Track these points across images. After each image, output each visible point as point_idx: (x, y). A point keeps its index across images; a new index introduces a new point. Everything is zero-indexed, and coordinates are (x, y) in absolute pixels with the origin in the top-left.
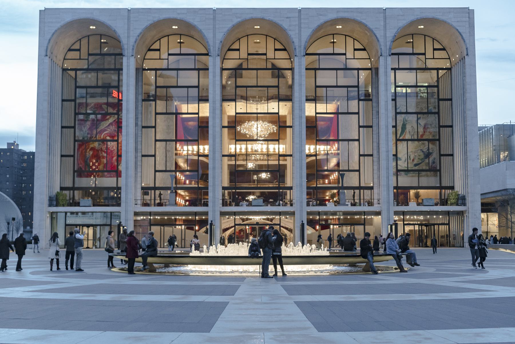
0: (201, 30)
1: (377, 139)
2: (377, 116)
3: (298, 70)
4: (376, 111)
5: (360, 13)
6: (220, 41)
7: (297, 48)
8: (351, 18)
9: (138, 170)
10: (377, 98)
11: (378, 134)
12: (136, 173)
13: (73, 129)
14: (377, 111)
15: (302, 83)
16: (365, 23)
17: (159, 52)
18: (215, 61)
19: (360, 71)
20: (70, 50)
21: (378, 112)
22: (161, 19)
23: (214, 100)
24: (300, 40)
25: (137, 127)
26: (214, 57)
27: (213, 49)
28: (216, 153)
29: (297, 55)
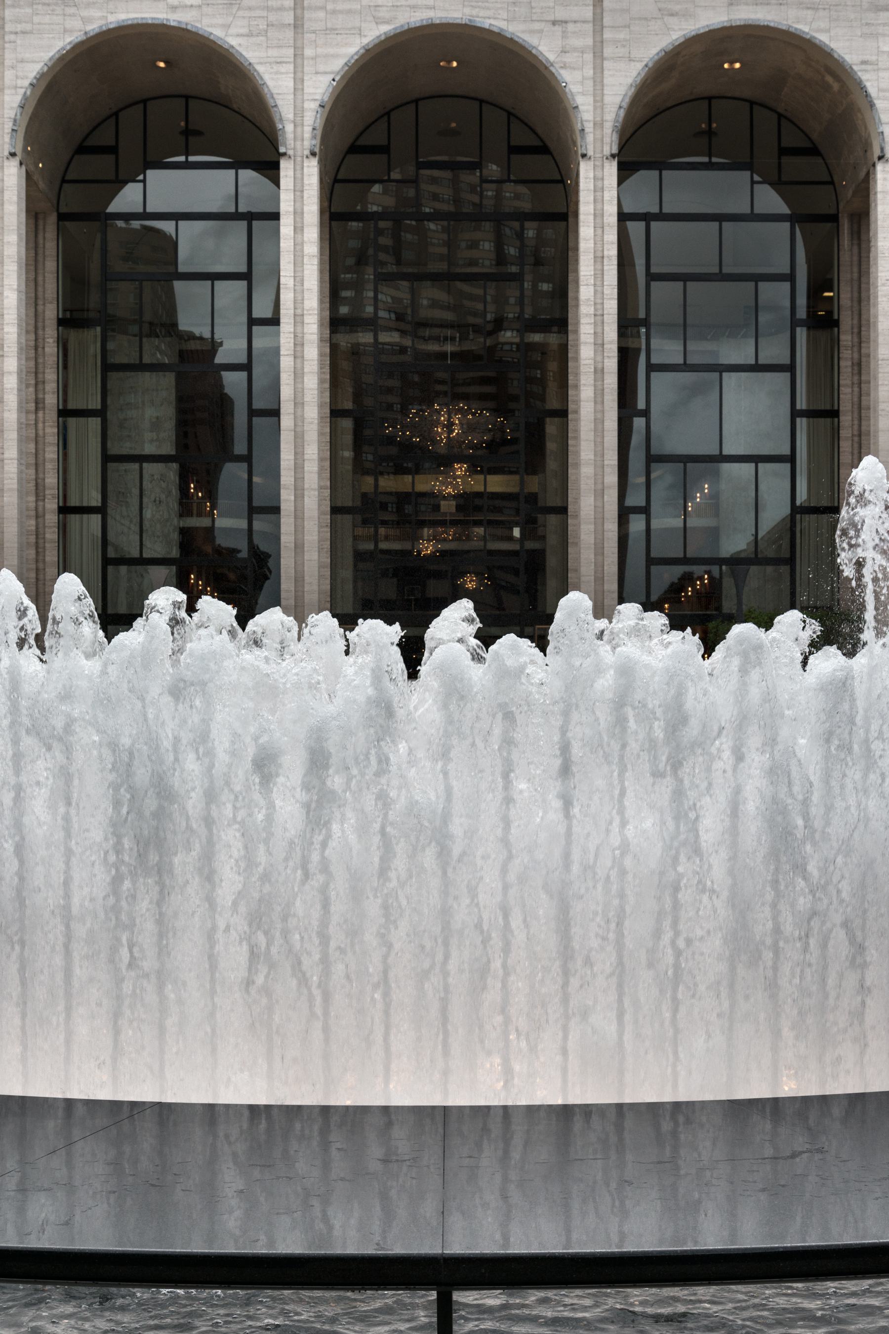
0: (250, 64)
1: (852, 454)
2: (856, 378)
3: (592, 207)
4: (852, 358)
5: (808, 8)
6: (318, 103)
7: (589, 128)
8: (776, 25)
9: (48, 559)
10: (856, 317)
11: (856, 439)
12: (41, 566)
13: (100, 516)
14: (856, 361)
15: (606, 253)
16: (827, 42)
17: (112, 157)
18: (302, 174)
19: (255, 223)
20: (82, 149)
21: (859, 364)
22: (111, 26)
23: (299, 312)
24: (599, 103)
25: (40, 414)
26: (299, 159)
27: (295, 132)
28: (306, 493)
29: (590, 153)
